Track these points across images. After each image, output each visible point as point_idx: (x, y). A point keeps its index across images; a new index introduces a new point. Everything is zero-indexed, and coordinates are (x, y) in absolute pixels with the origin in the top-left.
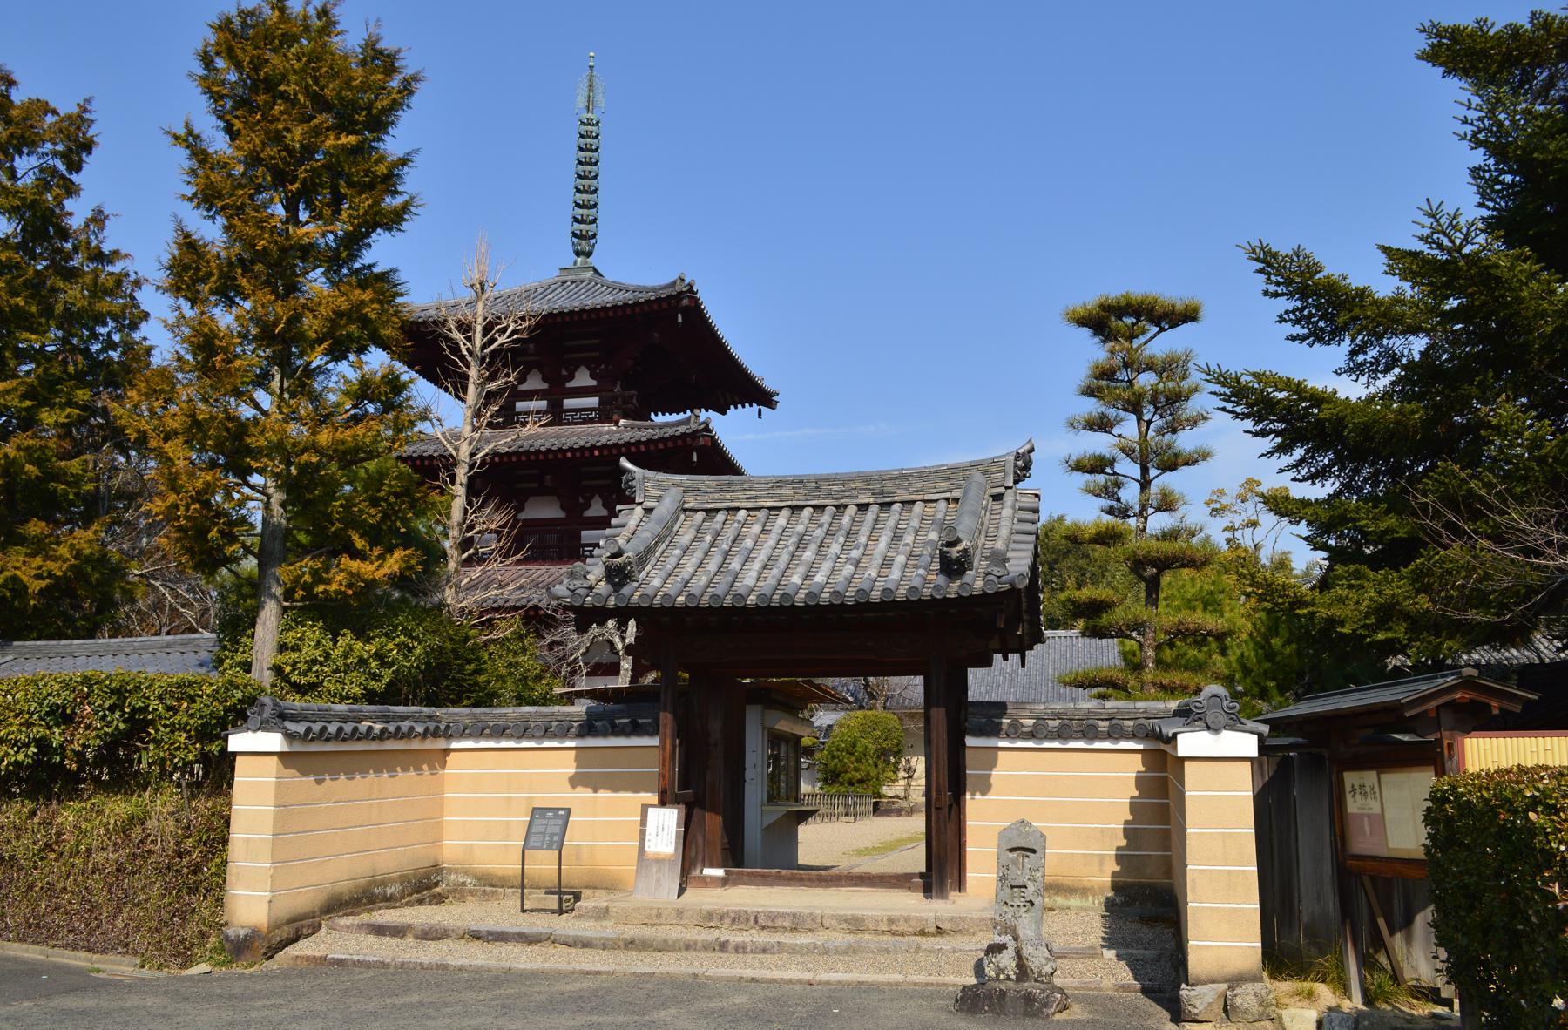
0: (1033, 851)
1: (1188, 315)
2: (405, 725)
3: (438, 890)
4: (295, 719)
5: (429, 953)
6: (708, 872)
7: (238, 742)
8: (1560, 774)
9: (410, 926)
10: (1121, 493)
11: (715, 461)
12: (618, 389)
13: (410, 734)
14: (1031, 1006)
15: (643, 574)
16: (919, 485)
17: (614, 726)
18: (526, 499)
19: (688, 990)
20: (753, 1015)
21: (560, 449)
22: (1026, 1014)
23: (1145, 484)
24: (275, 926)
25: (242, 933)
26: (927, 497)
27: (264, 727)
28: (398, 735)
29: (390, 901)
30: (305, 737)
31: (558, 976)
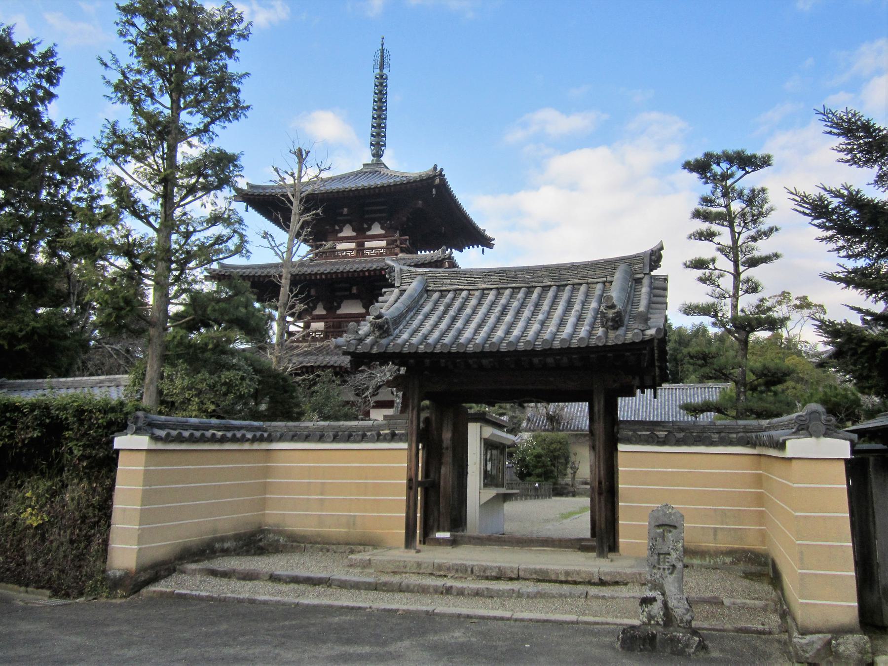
0: (675, 527)
1: (765, 161)
2: (209, 434)
3: (261, 544)
4: (161, 426)
5: (311, 598)
6: (439, 535)
7: (120, 442)
9: (234, 571)
10: (721, 281)
12: (397, 235)
13: (243, 440)
14: (676, 649)
15: (397, 331)
16: (585, 273)
17: (379, 435)
18: (342, 302)
19: (421, 624)
20: (464, 649)
21: (362, 271)
22: (673, 653)
23: (737, 275)
24: (141, 569)
25: (118, 574)
26: (590, 281)
27: (138, 431)
28: (234, 440)
29: (226, 552)
30: (168, 439)
31: (330, 610)
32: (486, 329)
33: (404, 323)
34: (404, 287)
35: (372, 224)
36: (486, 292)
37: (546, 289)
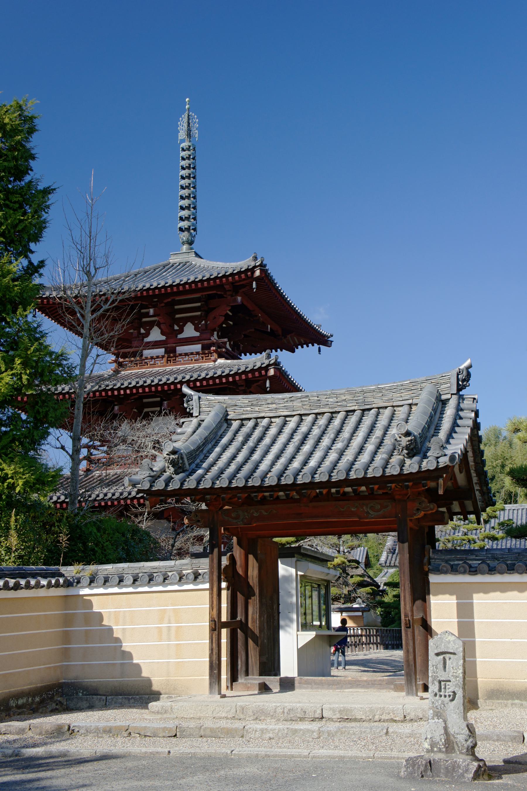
8: (0, 721)
11: (283, 384)
32: (283, 460)
33: (202, 456)
34: (202, 417)
35: (184, 325)
36: (288, 419)
37: (349, 413)
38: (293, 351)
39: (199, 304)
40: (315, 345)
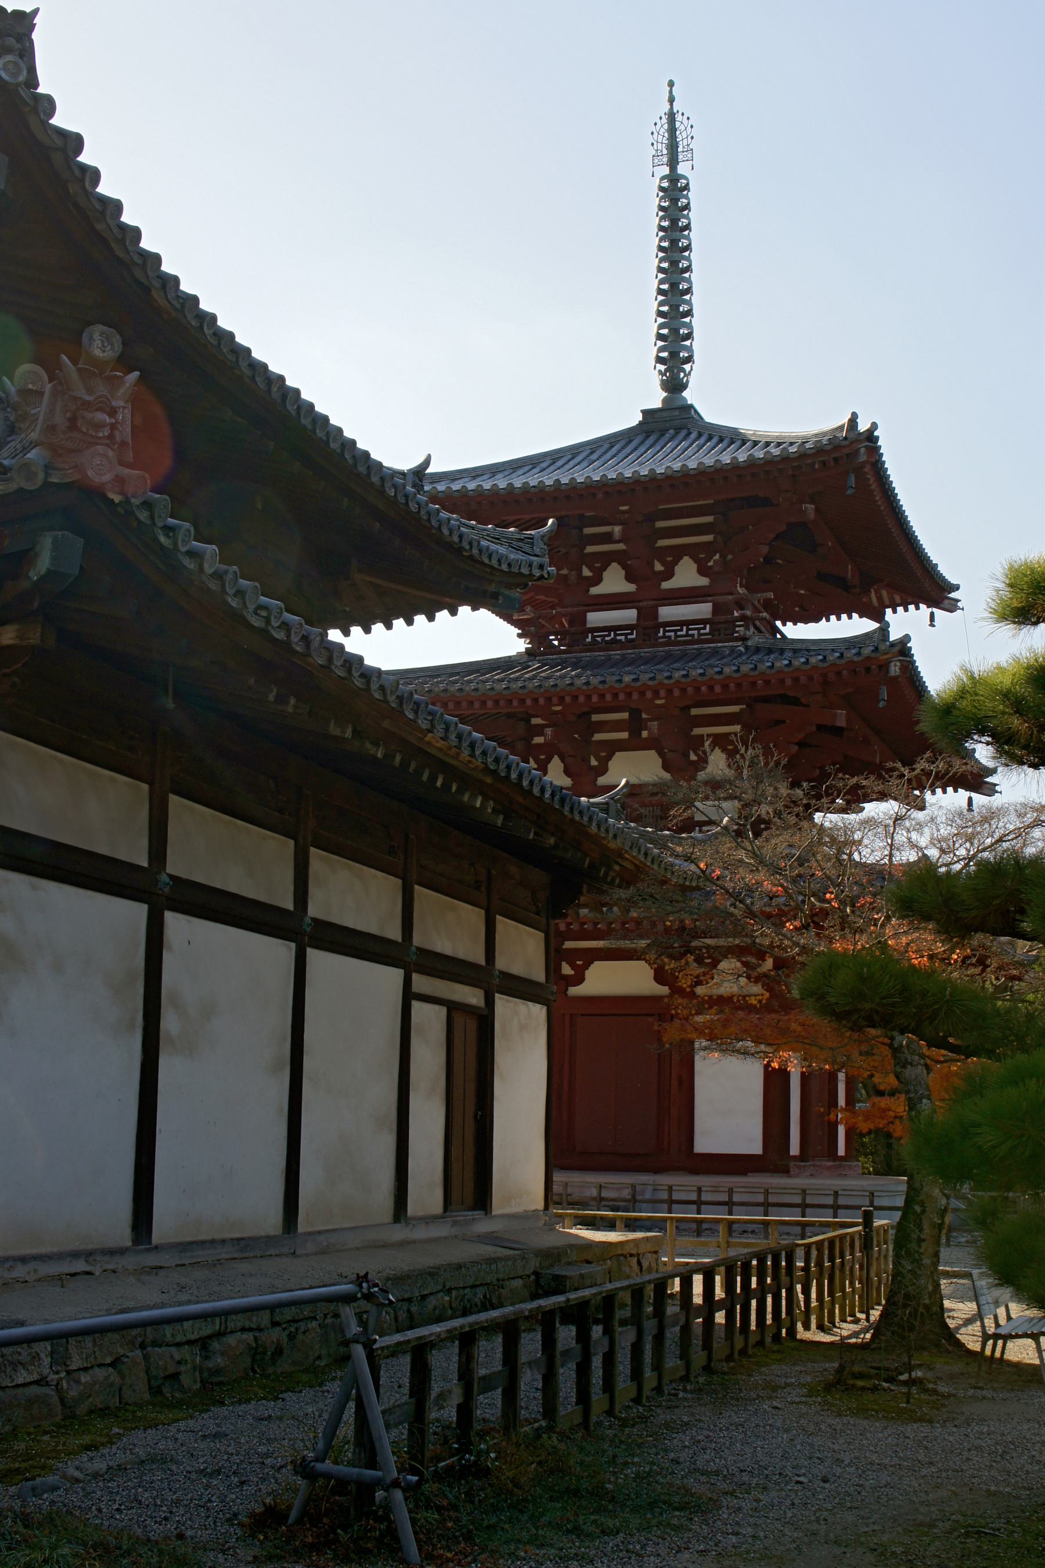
38: (645, 413)
39: (709, 519)
40: (922, 606)
